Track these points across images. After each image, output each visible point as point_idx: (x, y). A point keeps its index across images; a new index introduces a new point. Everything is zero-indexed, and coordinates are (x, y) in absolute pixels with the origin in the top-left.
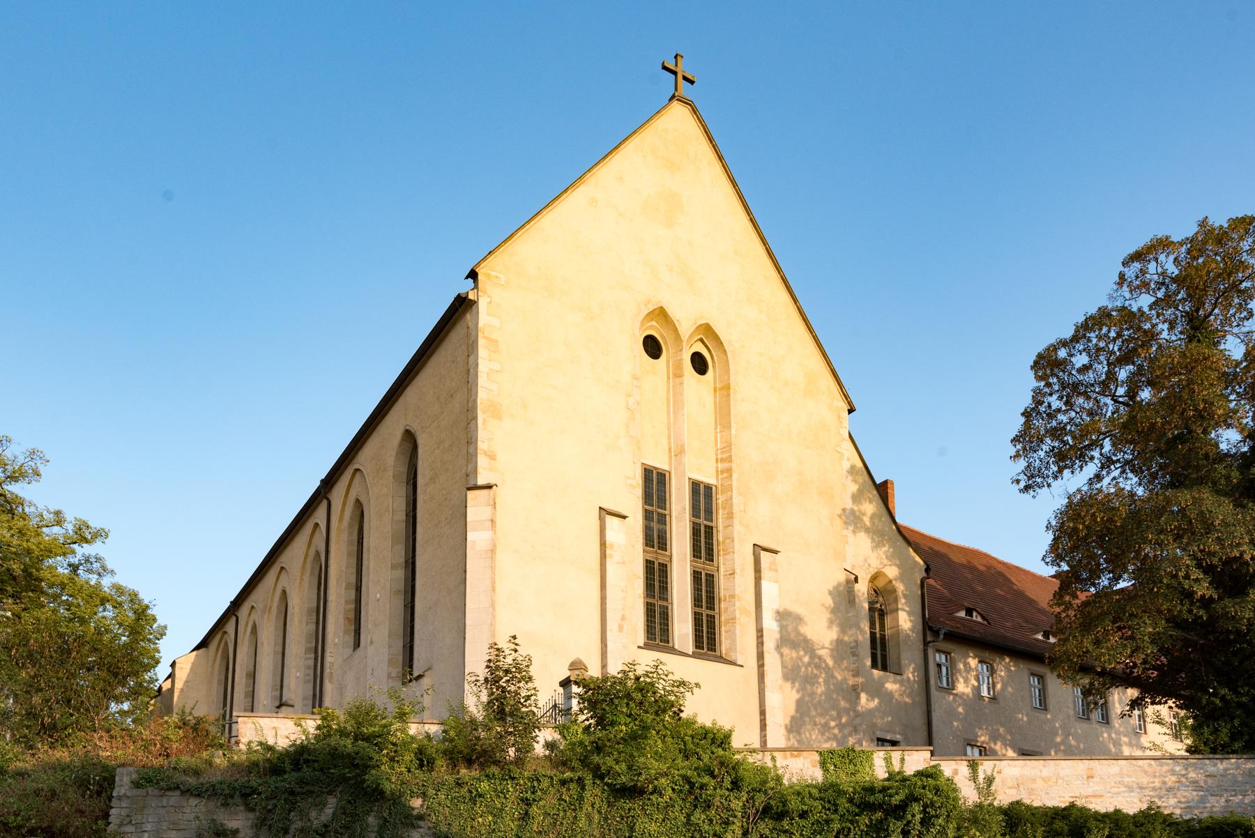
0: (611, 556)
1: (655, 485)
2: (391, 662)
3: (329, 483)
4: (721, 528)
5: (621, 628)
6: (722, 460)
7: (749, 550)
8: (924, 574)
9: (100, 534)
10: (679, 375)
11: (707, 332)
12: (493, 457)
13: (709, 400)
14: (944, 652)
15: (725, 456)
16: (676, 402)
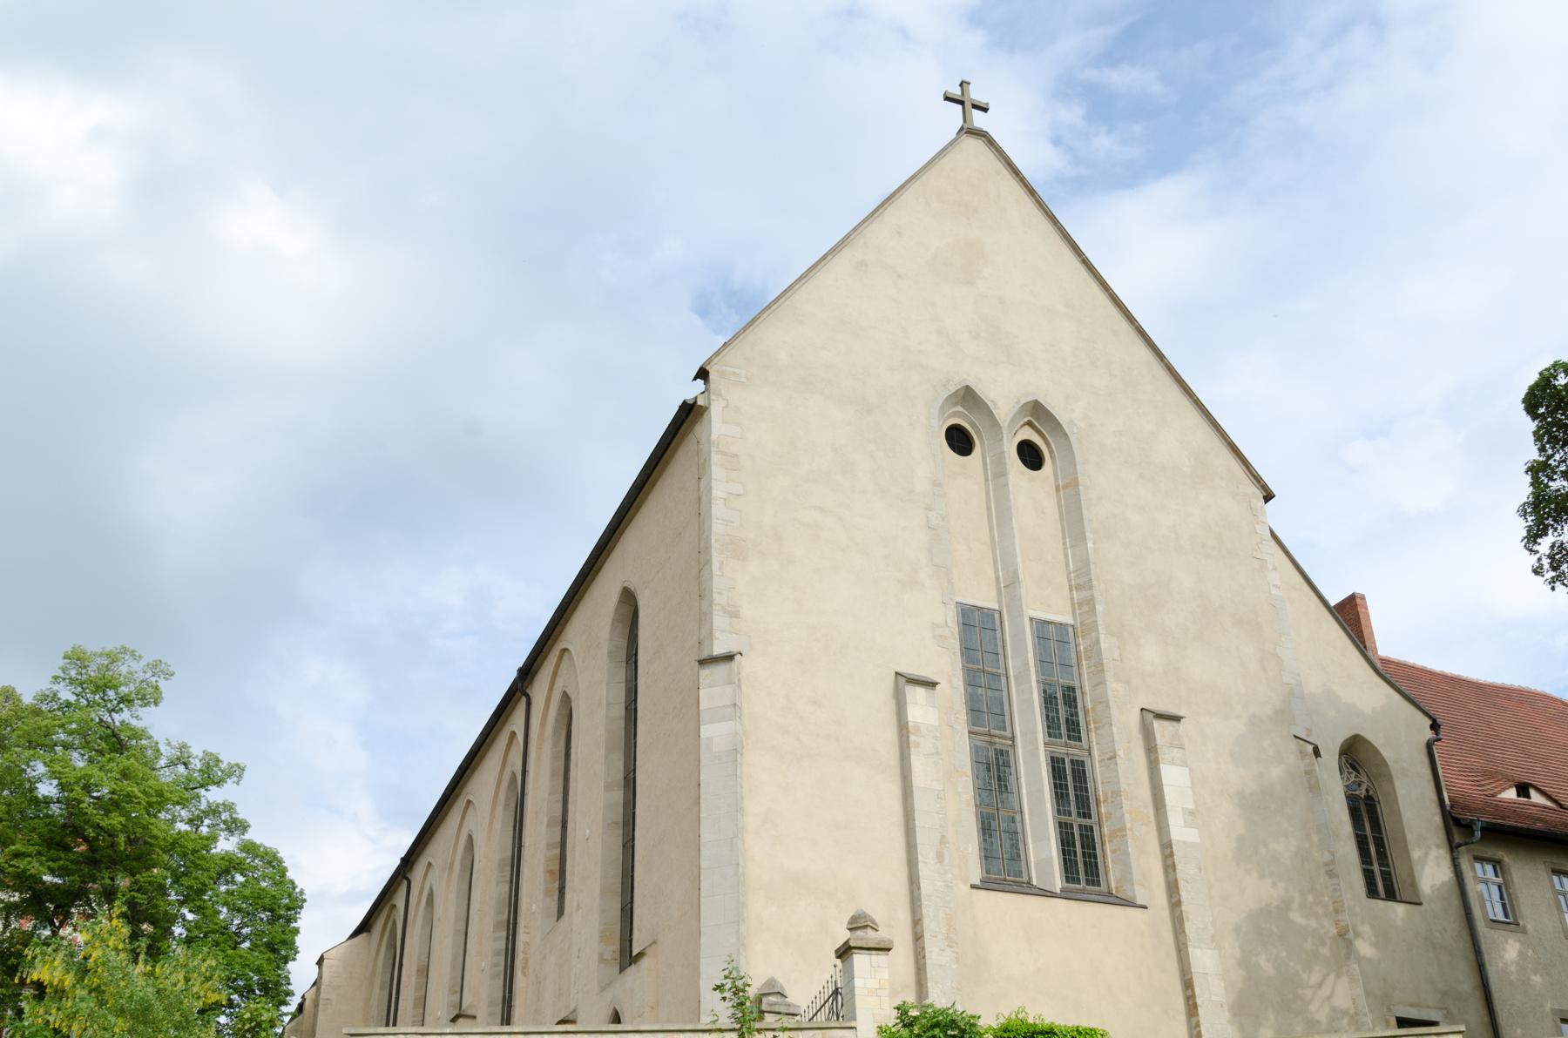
0: (918, 745)
1: (978, 632)
2: (604, 938)
3: (527, 673)
4: (1087, 688)
5: (940, 857)
6: (1078, 587)
7: (1134, 717)
8: (1430, 734)
9: (236, 771)
10: (1000, 474)
11: (1037, 413)
12: (735, 615)
13: (1050, 505)
14: (1488, 860)
15: (1081, 581)
16: (1000, 511)
